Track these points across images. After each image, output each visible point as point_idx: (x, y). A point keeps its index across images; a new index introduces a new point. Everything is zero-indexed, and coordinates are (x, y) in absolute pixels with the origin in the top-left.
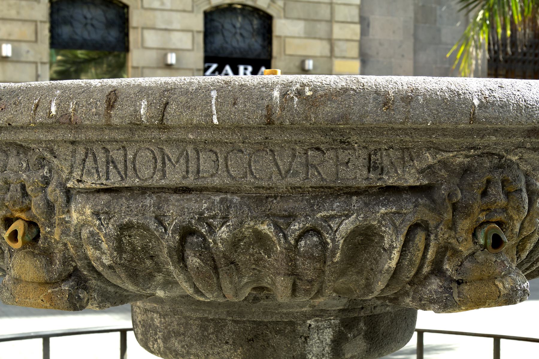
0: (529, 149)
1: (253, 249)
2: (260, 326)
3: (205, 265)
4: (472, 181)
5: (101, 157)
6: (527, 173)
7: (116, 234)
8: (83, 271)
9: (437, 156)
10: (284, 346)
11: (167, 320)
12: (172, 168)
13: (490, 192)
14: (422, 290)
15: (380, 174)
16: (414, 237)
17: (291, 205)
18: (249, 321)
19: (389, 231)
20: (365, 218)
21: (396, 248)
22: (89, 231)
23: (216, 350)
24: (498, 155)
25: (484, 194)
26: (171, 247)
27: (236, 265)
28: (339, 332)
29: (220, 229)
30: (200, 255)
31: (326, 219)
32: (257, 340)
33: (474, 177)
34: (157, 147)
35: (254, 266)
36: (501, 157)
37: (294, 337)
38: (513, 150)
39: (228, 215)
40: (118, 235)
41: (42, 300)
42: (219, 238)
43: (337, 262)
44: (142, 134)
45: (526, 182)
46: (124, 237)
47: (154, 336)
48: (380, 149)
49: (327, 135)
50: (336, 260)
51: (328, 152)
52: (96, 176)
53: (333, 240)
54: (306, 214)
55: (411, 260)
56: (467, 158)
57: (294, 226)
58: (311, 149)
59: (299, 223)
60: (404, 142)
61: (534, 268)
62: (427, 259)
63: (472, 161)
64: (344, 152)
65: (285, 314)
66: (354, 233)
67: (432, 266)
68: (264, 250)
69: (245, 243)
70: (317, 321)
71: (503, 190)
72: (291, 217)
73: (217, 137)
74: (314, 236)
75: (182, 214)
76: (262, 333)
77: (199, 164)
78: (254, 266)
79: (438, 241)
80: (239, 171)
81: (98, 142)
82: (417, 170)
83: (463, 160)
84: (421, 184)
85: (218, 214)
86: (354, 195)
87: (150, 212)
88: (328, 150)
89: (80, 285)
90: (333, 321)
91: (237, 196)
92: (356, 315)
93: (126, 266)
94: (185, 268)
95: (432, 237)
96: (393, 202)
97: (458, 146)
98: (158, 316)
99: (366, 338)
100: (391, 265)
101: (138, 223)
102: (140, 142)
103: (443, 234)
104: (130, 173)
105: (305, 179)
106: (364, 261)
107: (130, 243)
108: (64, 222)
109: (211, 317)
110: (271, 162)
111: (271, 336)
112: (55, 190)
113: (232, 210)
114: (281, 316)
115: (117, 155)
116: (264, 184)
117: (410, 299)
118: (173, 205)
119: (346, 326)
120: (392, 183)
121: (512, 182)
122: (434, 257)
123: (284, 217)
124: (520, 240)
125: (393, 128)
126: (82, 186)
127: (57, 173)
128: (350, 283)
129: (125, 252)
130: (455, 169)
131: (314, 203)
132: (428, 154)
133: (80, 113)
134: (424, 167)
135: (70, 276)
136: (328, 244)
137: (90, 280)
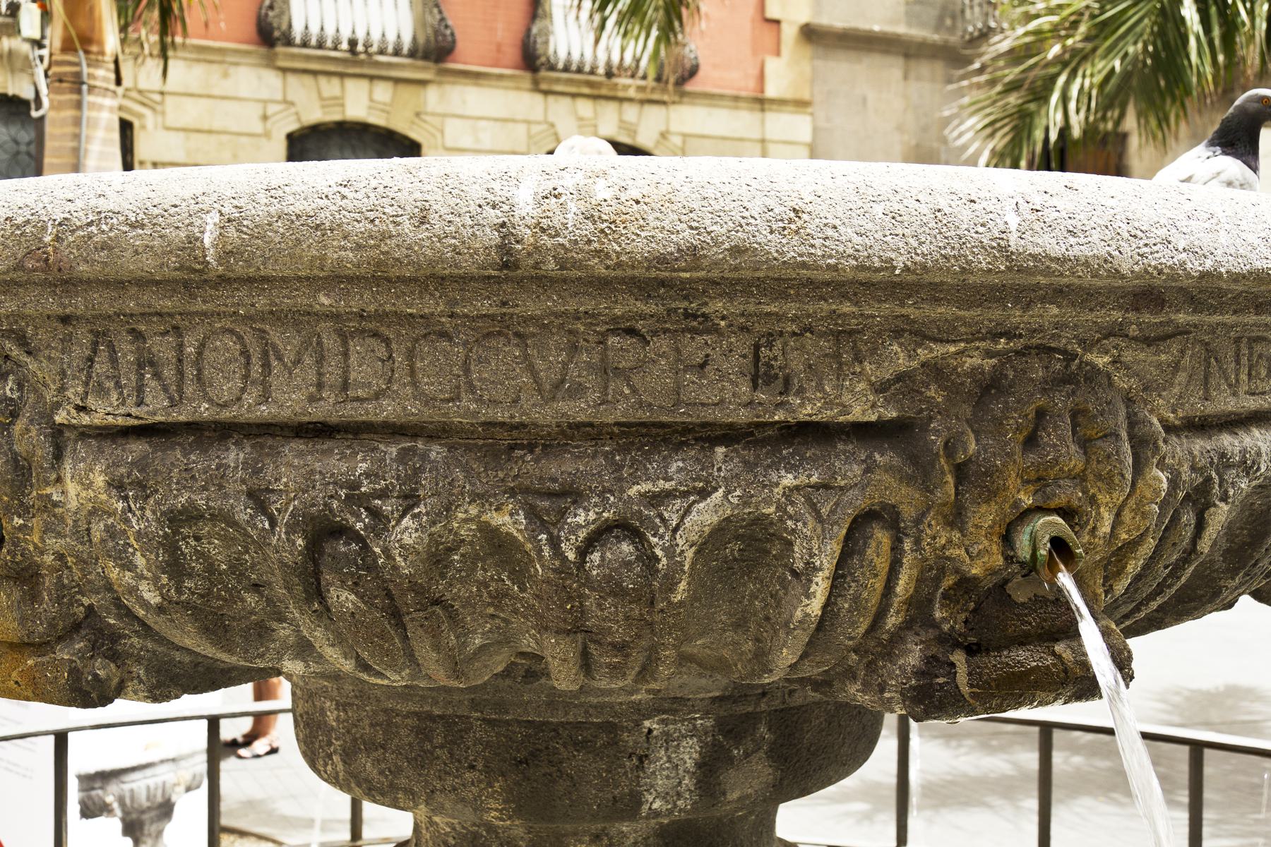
0: (1135, 339)
1: (485, 571)
2: (543, 731)
3: (370, 609)
4: (1002, 412)
5: (127, 352)
6: (1130, 395)
7: (161, 533)
8: (105, 617)
9: (919, 351)
10: (594, 776)
11: (350, 714)
12: (283, 377)
13: (1045, 440)
14: (885, 666)
15: (781, 394)
16: (865, 543)
17: (569, 467)
18: (519, 722)
19: (805, 530)
20: (745, 500)
21: (821, 569)
22: (106, 526)
23: (450, 781)
24: (1064, 352)
25: (1031, 442)
26: (286, 565)
27: (447, 607)
28: (714, 745)
29: (399, 522)
30: (356, 584)
31: (656, 499)
32: (536, 762)
33: (1007, 403)
34: (251, 327)
35: (491, 610)
36: (1070, 357)
37: (615, 756)
38: (1099, 340)
39: (417, 490)
40: (166, 535)
41: (16, 682)
42: (397, 545)
43: (681, 602)
44: (211, 296)
45: (1129, 417)
46: (184, 539)
47: (326, 748)
48: (781, 334)
49: (649, 296)
50: (678, 597)
51: (655, 339)
52: (116, 396)
53: (670, 551)
54: (603, 487)
55: (856, 599)
56: (991, 358)
57: (575, 515)
58: (614, 332)
59: (587, 510)
60: (839, 316)
61: (1142, 615)
62: (896, 596)
63: (1003, 364)
64: (692, 338)
65: (596, 707)
66: (720, 533)
67: (907, 611)
68: (510, 573)
69: (462, 555)
70: (662, 721)
71: (1074, 435)
72: (572, 495)
73: (389, 303)
74: (624, 540)
75: (308, 486)
76: (547, 748)
77: (348, 366)
78: (491, 610)
79: (921, 554)
80: (440, 383)
81: (119, 316)
82: (872, 384)
83: (980, 361)
84: (879, 417)
85: (394, 487)
86: (720, 445)
87: (236, 481)
88: (655, 333)
89: (99, 649)
90: (699, 722)
91: (440, 445)
92: (750, 709)
93: (196, 608)
94: (325, 613)
95: (907, 545)
96: (814, 461)
97: (968, 330)
98: (334, 707)
99: (772, 757)
100: (808, 610)
101: (209, 508)
102: (212, 315)
103: (934, 538)
104: (189, 390)
105: (600, 404)
106: (748, 600)
107: (201, 555)
108: (49, 505)
109: (437, 712)
110: (517, 363)
111: (565, 755)
112: (28, 430)
113: (426, 479)
114: (586, 712)
115: (162, 348)
116: (501, 415)
117: (858, 686)
118: (289, 465)
119: (728, 733)
120: (810, 415)
121: (1095, 417)
122: (911, 591)
123: (550, 495)
124: (1113, 553)
125: (810, 282)
126: (86, 419)
127: (36, 391)
128: (723, 648)
129: (190, 576)
130: (962, 384)
131: (622, 460)
132: (895, 347)
133: (69, 246)
134: (887, 377)
135: (76, 627)
136: (658, 560)
137: (125, 636)
